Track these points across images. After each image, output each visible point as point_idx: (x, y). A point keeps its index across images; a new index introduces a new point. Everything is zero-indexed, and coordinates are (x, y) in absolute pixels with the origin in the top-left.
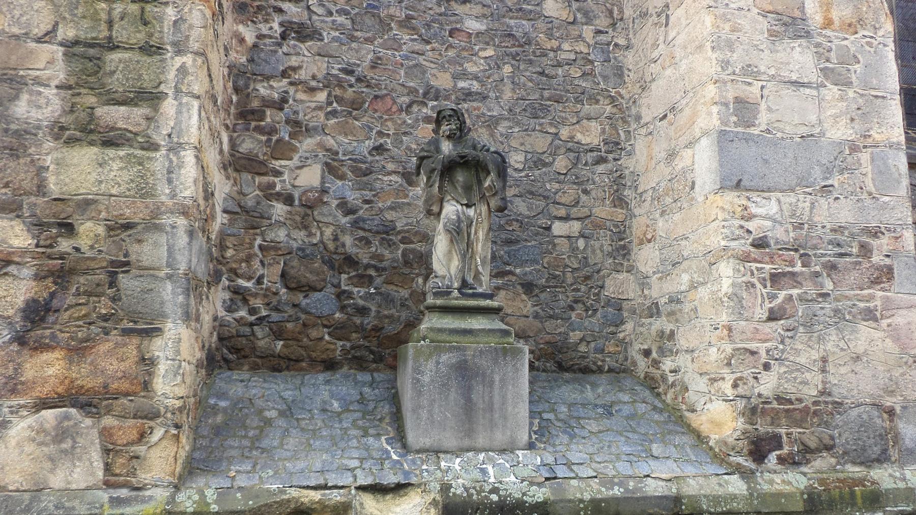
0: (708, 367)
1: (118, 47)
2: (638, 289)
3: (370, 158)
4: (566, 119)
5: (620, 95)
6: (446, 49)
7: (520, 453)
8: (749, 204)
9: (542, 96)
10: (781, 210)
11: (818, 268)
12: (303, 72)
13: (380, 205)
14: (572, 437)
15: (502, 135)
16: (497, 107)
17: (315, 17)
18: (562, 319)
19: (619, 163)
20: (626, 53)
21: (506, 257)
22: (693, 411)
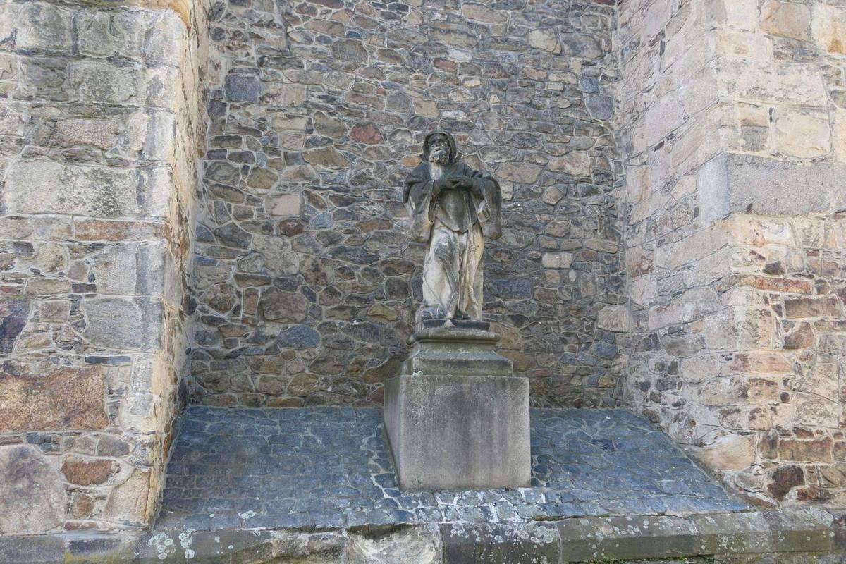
0: (720, 400)
1: (84, 57)
2: (632, 322)
3: (352, 188)
4: (555, 149)
5: (610, 127)
6: (430, 79)
7: (522, 490)
8: (760, 230)
9: (530, 126)
10: (795, 236)
11: (835, 296)
12: (281, 99)
13: (363, 235)
14: (575, 473)
15: (489, 164)
16: (484, 137)
17: (294, 45)
18: (554, 352)
19: (610, 194)
20: (615, 85)
21: (495, 288)
22: (702, 445)
